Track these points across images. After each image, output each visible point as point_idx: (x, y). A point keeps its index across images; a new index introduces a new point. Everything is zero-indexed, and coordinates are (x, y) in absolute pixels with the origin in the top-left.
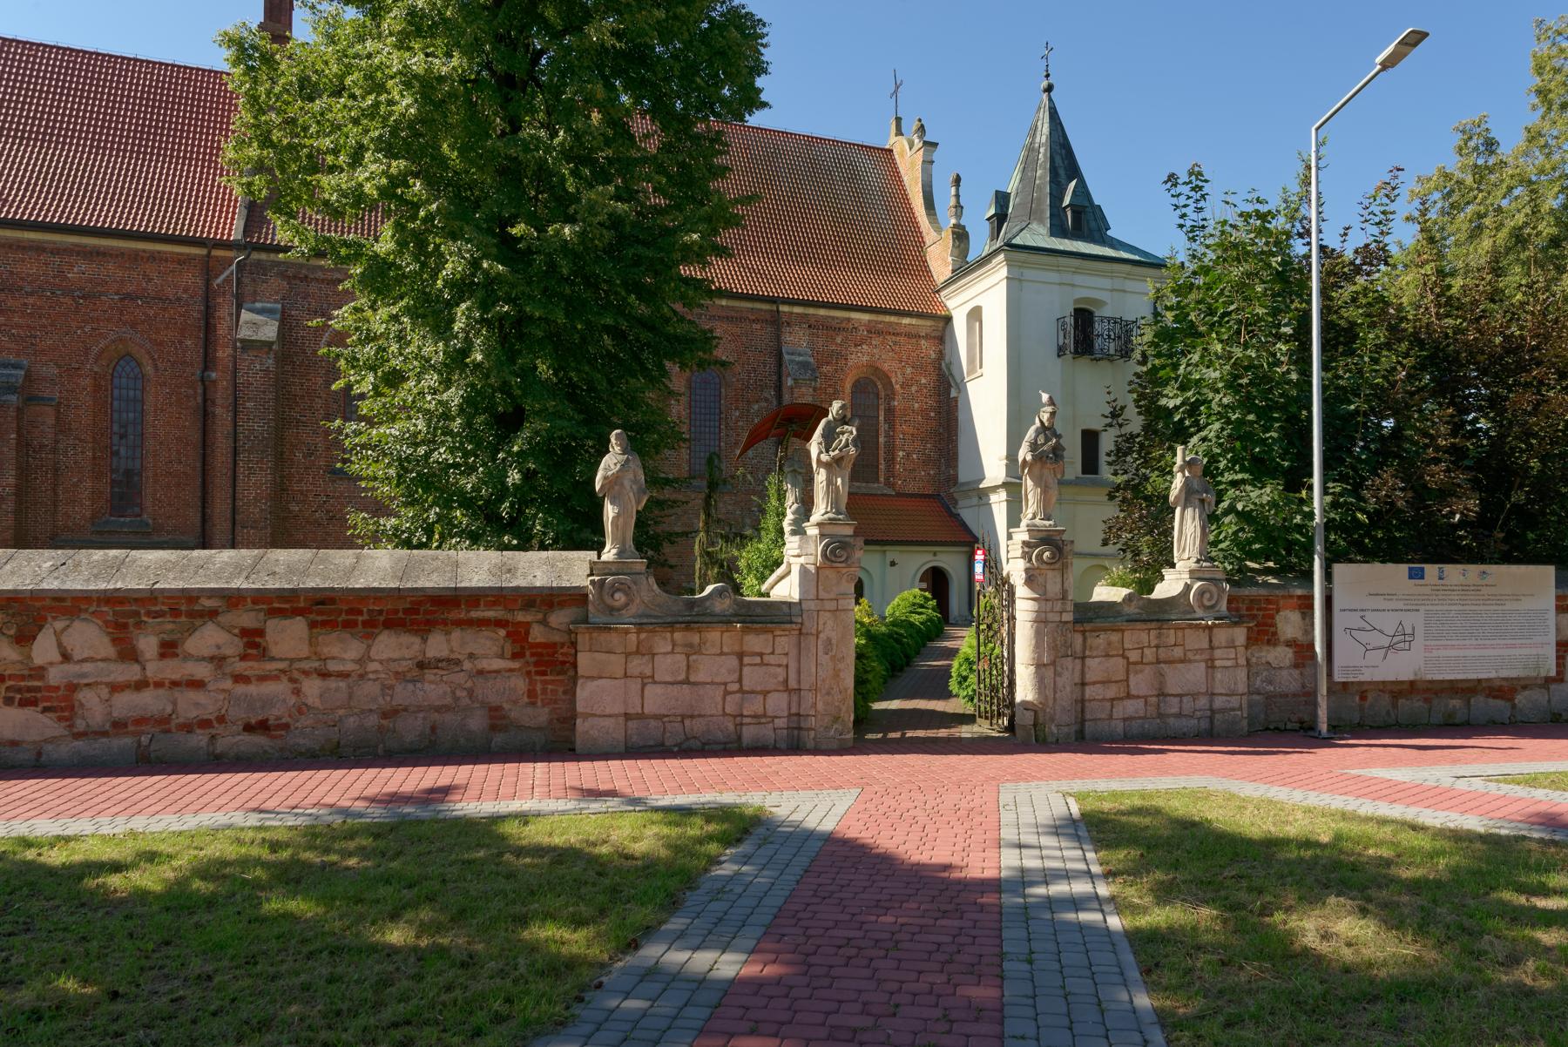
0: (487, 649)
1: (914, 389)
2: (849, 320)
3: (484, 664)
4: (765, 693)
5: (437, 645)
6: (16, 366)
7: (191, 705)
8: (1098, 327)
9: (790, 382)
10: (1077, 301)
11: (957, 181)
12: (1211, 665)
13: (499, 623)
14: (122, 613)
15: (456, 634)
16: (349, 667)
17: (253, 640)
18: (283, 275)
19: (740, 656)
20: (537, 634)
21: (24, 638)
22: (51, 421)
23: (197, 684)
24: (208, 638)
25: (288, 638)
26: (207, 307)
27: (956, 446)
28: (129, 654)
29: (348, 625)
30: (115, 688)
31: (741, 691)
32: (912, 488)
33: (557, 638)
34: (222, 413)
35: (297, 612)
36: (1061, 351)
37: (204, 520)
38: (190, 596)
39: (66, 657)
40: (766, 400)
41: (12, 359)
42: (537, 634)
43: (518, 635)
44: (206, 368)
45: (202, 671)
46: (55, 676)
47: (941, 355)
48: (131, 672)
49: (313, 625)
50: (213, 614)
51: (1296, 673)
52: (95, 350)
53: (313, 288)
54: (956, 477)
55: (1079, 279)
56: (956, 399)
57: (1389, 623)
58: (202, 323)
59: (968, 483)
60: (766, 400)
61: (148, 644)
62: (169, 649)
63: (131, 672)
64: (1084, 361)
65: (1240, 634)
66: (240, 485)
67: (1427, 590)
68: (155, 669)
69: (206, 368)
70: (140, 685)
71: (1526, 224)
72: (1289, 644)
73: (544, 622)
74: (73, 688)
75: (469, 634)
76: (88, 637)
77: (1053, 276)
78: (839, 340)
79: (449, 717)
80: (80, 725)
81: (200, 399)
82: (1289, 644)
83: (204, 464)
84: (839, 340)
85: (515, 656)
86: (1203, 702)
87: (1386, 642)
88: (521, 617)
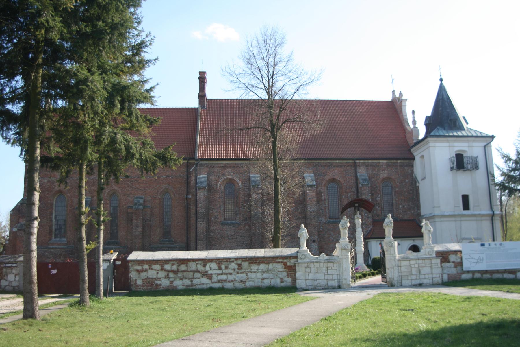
0: (279, 267)
1: (404, 184)
2: (379, 163)
3: (279, 270)
4: (332, 275)
5: (271, 266)
6: (141, 198)
7: (230, 278)
8: (465, 160)
9: (360, 185)
10: (456, 151)
11: (413, 112)
12: (431, 267)
13: (282, 262)
14: (219, 261)
15: (274, 264)
16: (256, 270)
17: (240, 265)
18: (207, 166)
19: (327, 268)
20: (289, 264)
21: (204, 266)
22: (149, 212)
23: (231, 274)
24: (233, 265)
25: (245, 264)
26: (187, 177)
27: (420, 203)
28: (220, 268)
29: (255, 263)
30: (218, 274)
31: (328, 274)
32: (406, 217)
33: (292, 265)
34: (192, 208)
35: (246, 261)
36: (452, 169)
37: (187, 239)
38: (230, 259)
39: (211, 269)
40: (353, 192)
41: (140, 196)
42: (289, 264)
43: (285, 264)
44: (187, 195)
45: (231, 271)
46: (210, 272)
47: (412, 172)
48: (220, 272)
49: (249, 263)
50: (233, 261)
51: (455, 269)
52: (160, 192)
53: (216, 170)
54: (420, 213)
55: (456, 144)
56: (418, 187)
57: (477, 257)
58: (186, 182)
59: (424, 215)
60: (353, 192)
61: (223, 267)
62: (226, 268)
63: (220, 272)
64: (460, 172)
65: (439, 261)
66: (198, 228)
67: (486, 249)
68: (224, 271)
69: (187, 195)
70: (222, 274)
71: (96, 342)
72: (454, 262)
73: (290, 262)
74: (212, 274)
75: (276, 264)
76: (214, 265)
77: (447, 144)
78: (376, 170)
79: (273, 280)
80: (213, 281)
81: (186, 204)
82: (454, 262)
83: (187, 222)
84: (376, 170)
85: (285, 268)
86: (430, 276)
87: (476, 261)
88: (285, 261)
